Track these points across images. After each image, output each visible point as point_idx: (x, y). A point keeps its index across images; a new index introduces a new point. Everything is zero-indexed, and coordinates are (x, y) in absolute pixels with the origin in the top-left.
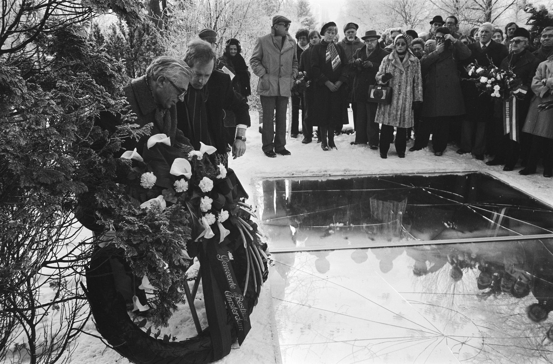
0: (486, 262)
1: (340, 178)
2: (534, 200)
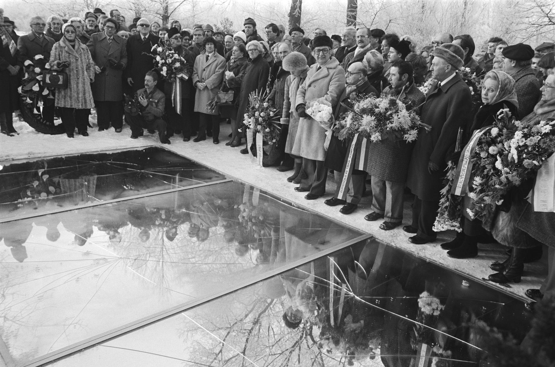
0: (154, 208)
1: (25, 161)
2: (194, 162)
